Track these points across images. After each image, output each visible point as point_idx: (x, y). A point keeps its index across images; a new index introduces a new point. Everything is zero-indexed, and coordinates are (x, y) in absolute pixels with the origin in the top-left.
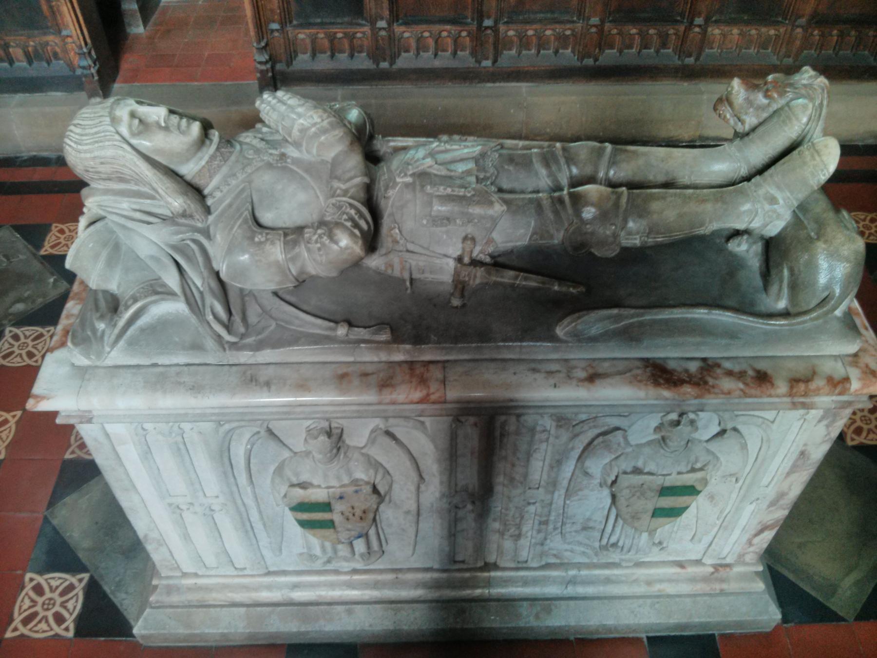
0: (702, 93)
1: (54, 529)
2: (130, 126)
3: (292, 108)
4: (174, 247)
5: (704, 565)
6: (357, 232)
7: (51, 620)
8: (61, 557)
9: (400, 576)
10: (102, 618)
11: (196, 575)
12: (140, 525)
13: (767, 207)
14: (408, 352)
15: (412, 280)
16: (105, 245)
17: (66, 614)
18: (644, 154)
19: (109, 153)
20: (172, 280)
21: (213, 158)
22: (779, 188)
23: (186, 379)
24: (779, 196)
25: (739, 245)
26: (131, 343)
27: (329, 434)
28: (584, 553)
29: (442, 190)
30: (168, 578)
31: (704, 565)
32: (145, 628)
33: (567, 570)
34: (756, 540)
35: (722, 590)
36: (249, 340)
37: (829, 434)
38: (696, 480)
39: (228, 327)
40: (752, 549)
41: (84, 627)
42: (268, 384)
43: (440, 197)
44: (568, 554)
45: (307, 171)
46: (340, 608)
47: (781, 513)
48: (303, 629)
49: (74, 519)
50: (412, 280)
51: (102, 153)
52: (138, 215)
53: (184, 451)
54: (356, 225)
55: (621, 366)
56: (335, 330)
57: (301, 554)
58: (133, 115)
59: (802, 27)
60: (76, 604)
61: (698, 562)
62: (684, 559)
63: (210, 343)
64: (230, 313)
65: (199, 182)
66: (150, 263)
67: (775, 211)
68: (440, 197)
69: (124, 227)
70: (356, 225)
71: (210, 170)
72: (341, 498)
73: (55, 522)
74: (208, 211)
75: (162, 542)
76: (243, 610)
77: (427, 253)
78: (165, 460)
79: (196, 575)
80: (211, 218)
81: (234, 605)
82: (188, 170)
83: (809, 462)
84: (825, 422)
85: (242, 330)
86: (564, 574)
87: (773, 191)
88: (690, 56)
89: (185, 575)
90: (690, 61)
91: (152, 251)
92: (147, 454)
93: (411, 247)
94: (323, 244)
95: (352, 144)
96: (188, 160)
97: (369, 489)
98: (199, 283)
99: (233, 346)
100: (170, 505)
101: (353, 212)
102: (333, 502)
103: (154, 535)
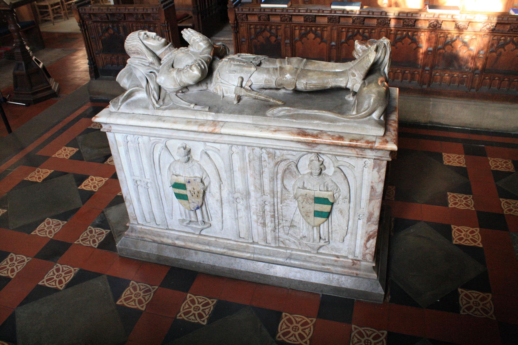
0: (430, 101)
1: (104, 215)
2: (143, 37)
3: (192, 34)
4: (147, 75)
5: (348, 258)
6: (199, 67)
7: (91, 242)
8: (104, 224)
9: (217, 240)
10: (109, 244)
11: (143, 225)
12: (124, 192)
13: (352, 78)
14: (213, 116)
15: (223, 97)
16: (128, 73)
17: (97, 241)
18: (317, 63)
19: (135, 43)
20: (144, 84)
21: (166, 49)
22: (356, 70)
23: (141, 117)
24: (356, 73)
25: (349, 97)
26: (127, 104)
27: (185, 148)
28: (294, 242)
29: (236, 63)
30: (133, 224)
31: (348, 258)
32: (121, 245)
33: (286, 250)
34: (368, 245)
35: (357, 274)
36: (163, 107)
37: (380, 177)
38: (328, 195)
39: (157, 102)
40: (367, 251)
41: (102, 246)
42: (164, 121)
43: (234, 65)
44: (287, 242)
45: (194, 54)
46: (193, 251)
47: (375, 228)
48: (177, 257)
49: (112, 214)
50: (223, 97)
51: (133, 43)
52: (140, 64)
53: (139, 152)
54: (200, 65)
55: (288, 129)
56: (190, 105)
57: (180, 220)
58: (145, 34)
59: (478, 74)
60: (102, 238)
61: (346, 257)
62: (340, 254)
63: (151, 106)
64: (159, 98)
65: (160, 56)
66: (139, 79)
67: (355, 79)
68: (234, 65)
69: (135, 67)
70: (200, 65)
71: (164, 53)
72: (189, 182)
73: (105, 213)
74: (161, 64)
75: (131, 203)
76: (156, 244)
77: (226, 83)
78: (133, 155)
79: (143, 225)
80: (161, 66)
81: (154, 241)
82: (158, 53)
83: (377, 194)
84: (376, 169)
85: (162, 104)
86: (285, 251)
87: (354, 72)
88: (425, 84)
89: (138, 224)
90: (425, 87)
91: (141, 75)
92: (127, 151)
93: (222, 81)
94: (188, 71)
95: (209, 46)
96: (159, 49)
97: (199, 180)
98: (152, 87)
99: (158, 109)
100: (134, 180)
101: (200, 62)
102: (186, 184)
103: (128, 197)
